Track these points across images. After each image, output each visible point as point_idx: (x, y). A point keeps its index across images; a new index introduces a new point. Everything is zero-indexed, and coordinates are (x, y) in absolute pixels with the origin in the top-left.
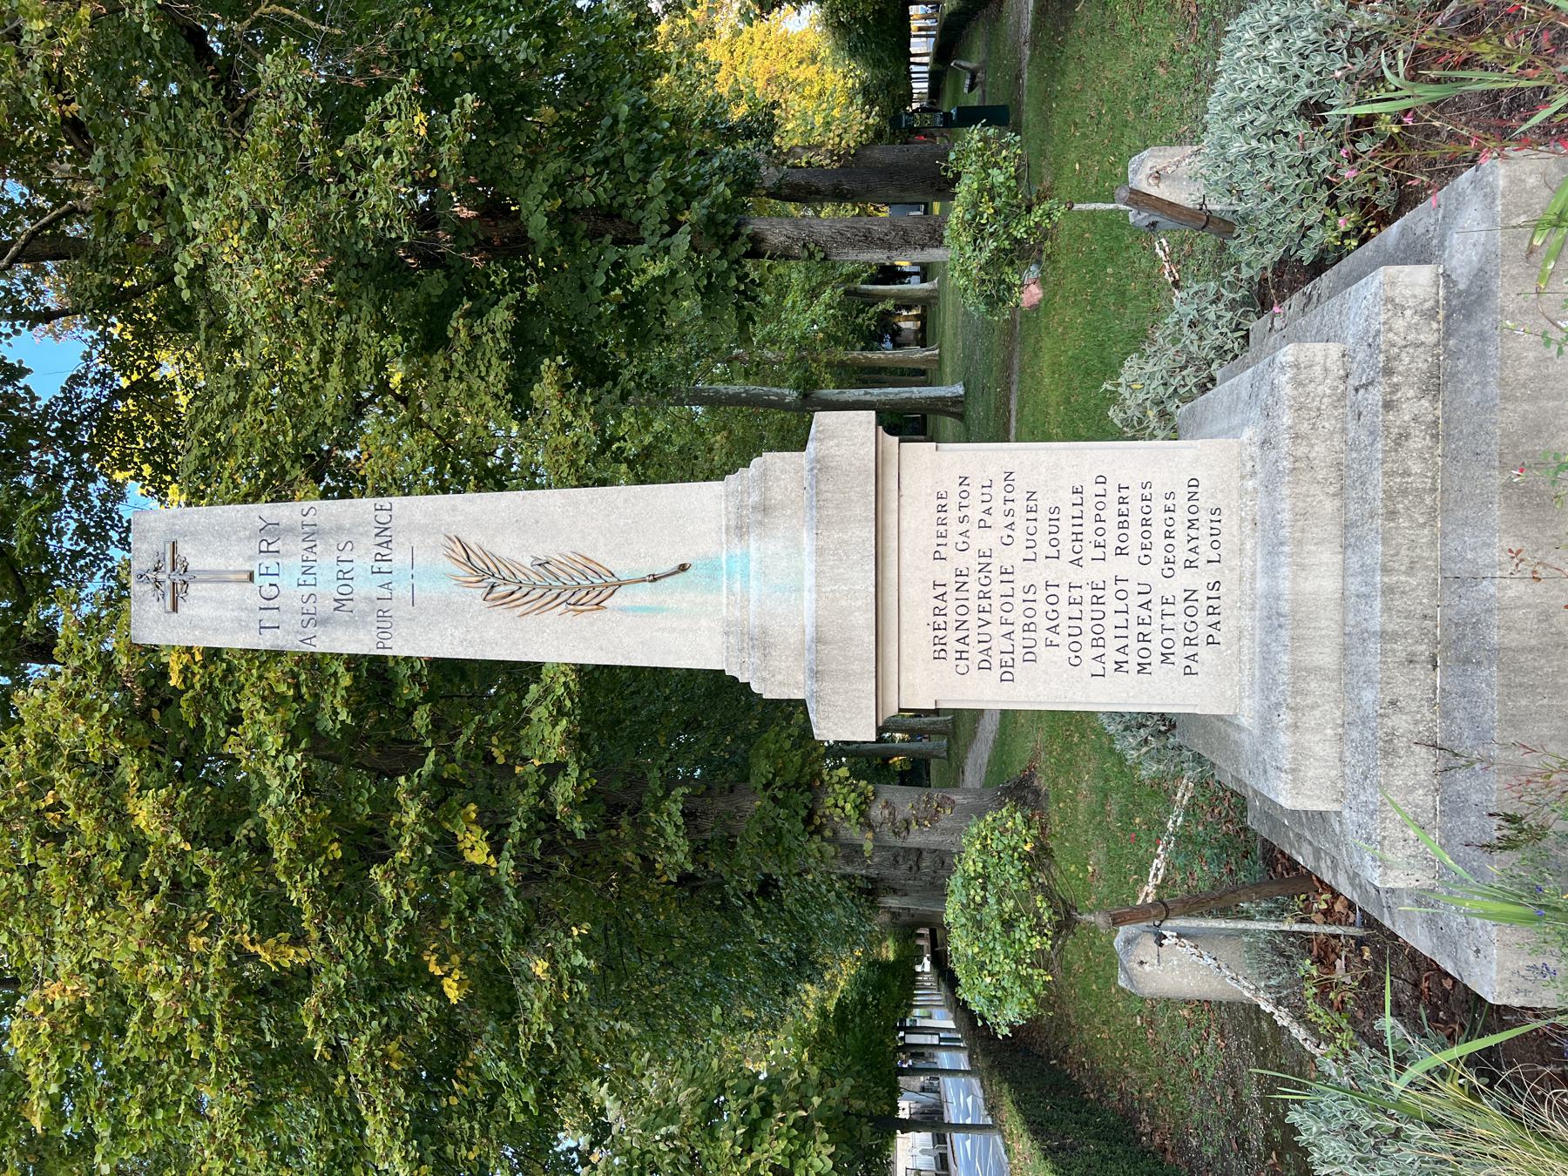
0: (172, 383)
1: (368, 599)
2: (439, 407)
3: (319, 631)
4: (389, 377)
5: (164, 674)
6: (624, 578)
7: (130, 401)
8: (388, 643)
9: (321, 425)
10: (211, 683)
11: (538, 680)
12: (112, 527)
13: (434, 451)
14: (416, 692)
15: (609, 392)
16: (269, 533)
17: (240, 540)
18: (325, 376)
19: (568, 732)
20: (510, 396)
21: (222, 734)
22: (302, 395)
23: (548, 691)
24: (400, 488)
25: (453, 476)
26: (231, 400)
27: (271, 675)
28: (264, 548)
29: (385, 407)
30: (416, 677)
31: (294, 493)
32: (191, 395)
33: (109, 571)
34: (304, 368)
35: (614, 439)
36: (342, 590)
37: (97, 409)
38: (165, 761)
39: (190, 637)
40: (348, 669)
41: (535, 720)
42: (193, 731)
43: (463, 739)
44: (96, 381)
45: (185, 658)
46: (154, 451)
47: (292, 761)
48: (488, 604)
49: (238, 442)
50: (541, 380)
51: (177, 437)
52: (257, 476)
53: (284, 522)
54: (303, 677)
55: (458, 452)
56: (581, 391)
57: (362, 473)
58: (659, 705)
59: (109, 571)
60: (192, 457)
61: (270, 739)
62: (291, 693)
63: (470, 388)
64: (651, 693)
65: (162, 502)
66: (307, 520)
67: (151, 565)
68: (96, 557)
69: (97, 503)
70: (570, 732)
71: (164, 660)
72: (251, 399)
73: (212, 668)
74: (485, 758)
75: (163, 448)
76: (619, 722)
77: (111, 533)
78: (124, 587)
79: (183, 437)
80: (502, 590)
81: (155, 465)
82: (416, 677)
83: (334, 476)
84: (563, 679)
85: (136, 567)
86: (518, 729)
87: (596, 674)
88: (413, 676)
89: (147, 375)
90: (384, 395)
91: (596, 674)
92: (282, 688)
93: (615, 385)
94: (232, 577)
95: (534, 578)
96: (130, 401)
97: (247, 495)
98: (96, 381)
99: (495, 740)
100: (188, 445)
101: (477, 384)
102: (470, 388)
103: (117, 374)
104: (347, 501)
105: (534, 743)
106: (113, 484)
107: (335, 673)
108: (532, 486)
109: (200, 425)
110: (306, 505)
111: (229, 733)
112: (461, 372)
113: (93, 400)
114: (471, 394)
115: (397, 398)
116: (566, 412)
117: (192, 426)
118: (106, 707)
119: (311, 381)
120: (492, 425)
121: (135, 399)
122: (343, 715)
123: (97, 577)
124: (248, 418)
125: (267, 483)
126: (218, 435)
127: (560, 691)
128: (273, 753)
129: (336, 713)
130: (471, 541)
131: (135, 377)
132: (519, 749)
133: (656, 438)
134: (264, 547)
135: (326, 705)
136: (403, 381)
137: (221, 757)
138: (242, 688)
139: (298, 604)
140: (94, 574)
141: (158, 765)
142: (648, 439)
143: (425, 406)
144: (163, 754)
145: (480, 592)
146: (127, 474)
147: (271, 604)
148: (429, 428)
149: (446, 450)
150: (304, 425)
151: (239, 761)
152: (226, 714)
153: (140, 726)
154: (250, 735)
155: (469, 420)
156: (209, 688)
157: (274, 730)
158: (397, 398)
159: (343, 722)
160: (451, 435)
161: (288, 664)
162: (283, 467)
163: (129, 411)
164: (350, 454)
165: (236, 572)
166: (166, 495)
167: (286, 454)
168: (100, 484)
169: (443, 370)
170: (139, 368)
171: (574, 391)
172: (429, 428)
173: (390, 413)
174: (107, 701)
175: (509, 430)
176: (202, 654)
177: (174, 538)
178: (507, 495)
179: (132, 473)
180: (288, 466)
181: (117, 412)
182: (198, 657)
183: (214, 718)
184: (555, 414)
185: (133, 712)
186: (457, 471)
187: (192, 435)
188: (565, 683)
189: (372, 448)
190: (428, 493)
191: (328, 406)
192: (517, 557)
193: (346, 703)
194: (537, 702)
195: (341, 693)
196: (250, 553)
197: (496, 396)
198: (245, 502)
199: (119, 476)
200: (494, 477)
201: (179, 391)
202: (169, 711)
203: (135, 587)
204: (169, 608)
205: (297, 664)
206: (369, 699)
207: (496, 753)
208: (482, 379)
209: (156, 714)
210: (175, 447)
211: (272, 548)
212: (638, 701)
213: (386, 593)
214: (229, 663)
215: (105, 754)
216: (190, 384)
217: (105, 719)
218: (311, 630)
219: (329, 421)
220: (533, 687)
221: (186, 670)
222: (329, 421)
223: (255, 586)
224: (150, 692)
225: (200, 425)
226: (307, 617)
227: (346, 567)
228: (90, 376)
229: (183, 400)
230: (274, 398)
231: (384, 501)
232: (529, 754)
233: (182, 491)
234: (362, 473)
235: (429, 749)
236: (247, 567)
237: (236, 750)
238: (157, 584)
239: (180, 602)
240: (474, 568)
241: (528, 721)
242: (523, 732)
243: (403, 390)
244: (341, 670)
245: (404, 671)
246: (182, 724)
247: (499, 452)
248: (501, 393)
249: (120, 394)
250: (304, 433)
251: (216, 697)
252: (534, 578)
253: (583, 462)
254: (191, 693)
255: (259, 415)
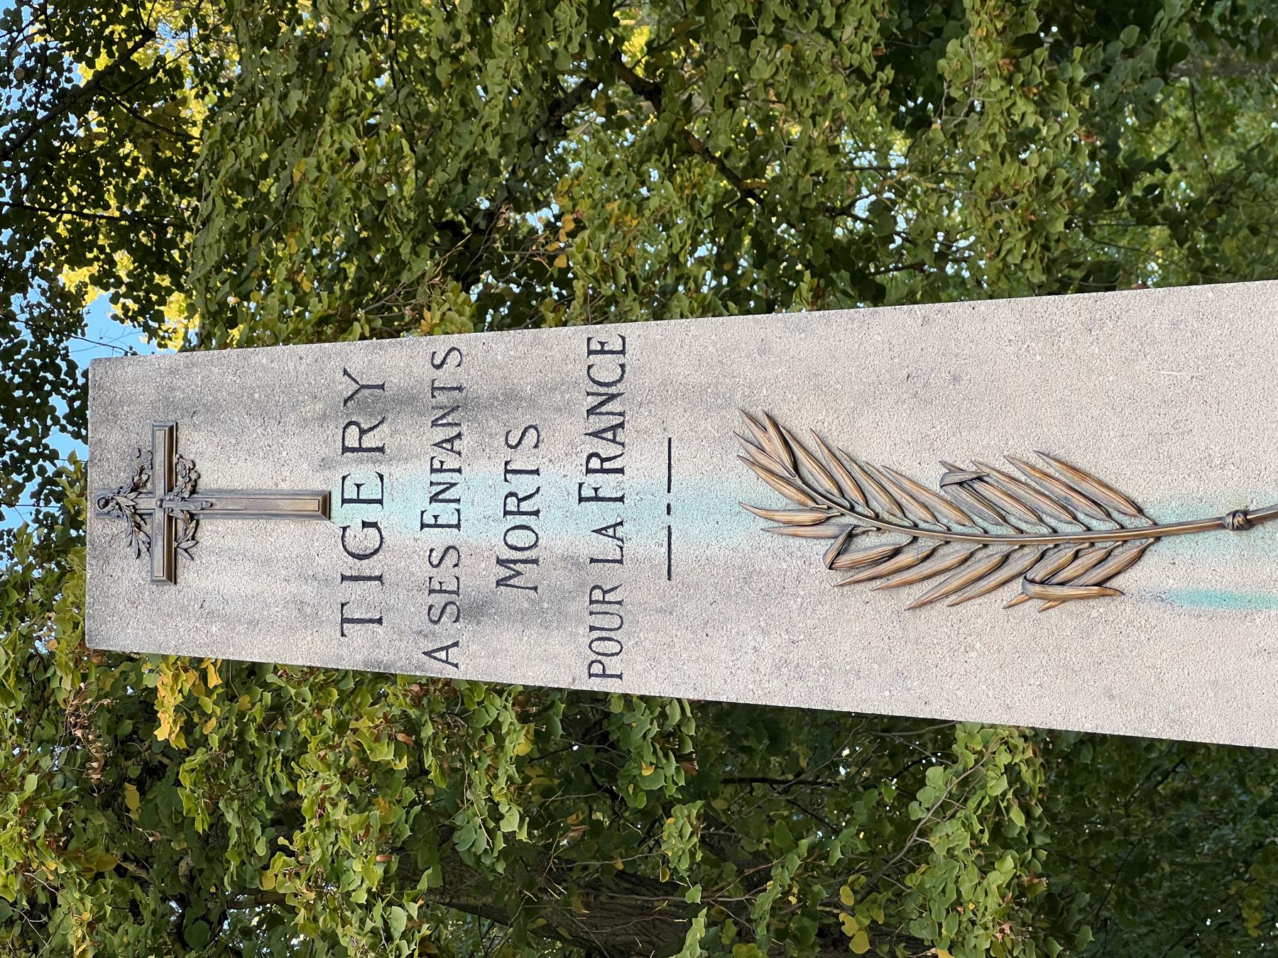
0: (176, 74)
1: (571, 562)
2: (730, 104)
3: (464, 632)
4: (620, 40)
5: (146, 709)
6: (1168, 517)
7: (93, 115)
8: (613, 665)
9: (475, 158)
10: (241, 734)
11: (949, 758)
12: (55, 389)
13: (716, 207)
14: (670, 777)
15: (1129, 53)
16: (364, 407)
17: (305, 422)
18: (484, 46)
19: (1018, 890)
20: (888, 74)
21: (261, 849)
22: (436, 88)
23: (967, 784)
24: (645, 297)
25: (758, 264)
26: (293, 107)
27: (364, 724)
28: (352, 441)
29: (611, 109)
30: (668, 739)
31: (419, 310)
32: (212, 98)
33: (48, 481)
34: (441, 29)
35: (1139, 165)
36: (514, 538)
37: (30, 133)
38: (150, 901)
39: (201, 638)
40: (523, 718)
41: (940, 852)
42: (204, 839)
43: (773, 890)
44: (27, 74)
45: (189, 680)
46: (137, 222)
47: (399, 920)
48: (838, 577)
49: (306, 200)
50: (964, 29)
51: (182, 189)
52: (340, 275)
53: (395, 381)
54: (428, 731)
55: (768, 208)
56: (1059, 52)
57: (561, 262)
58: (1245, 826)
59: (48, 481)
60: (213, 235)
61: (357, 866)
62: (403, 765)
63: (798, 57)
64: (1225, 795)
65: (152, 333)
66: (444, 377)
67: (124, 478)
68: (23, 450)
69: (27, 335)
70: (1022, 890)
71: (149, 681)
72: (333, 104)
73: (244, 700)
74: (822, 933)
75: (154, 218)
76: (1143, 865)
77: (55, 400)
78: (75, 520)
79: (195, 190)
80: (871, 544)
81: (140, 254)
82: (668, 739)
83: (501, 273)
84: (1004, 759)
85: (98, 481)
86: (902, 870)
87: (1086, 757)
88: (664, 737)
89: (126, 56)
90: (609, 83)
91: (1086, 757)
92: (385, 753)
93: (1146, 31)
94: (286, 505)
95: (949, 516)
96: (93, 115)
97: (323, 321)
98: (27, 74)
99: (846, 897)
100: (204, 208)
101: (814, 47)
102: (798, 57)
103: (67, 57)
104: (530, 334)
105: (939, 910)
106: (58, 295)
107: (497, 724)
108: (935, 291)
109: (229, 165)
110: (441, 343)
111: (274, 848)
112: (779, 22)
113: (22, 114)
114: (800, 72)
115: (640, 87)
116: (1022, 106)
117: (214, 162)
118: (32, 781)
119: (455, 58)
120: (846, 141)
121: (103, 109)
122: (512, 822)
123: (25, 497)
124: (326, 148)
125: (362, 286)
126: (264, 186)
127: (998, 785)
128: (362, 898)
129: (497, 816)
130: (801, 424)
131: (102, 62)
132: (903, 918)
133: (1244, 158)
134: (352, 439)
135: (476, 796)
136: (651, 48)
137: (260, 897)
138: (303, 746)
139: (421, 570)
140: (19, 488)
141: (135, 908)
142: (1223, 161)
143: (698, 102)
144: (144, 884)
145: (821, 549)
146: (83, 274)
147: (366, 567)
148: (707, 154)
149: (742, 203)
150: (440, 160)
151: (293, 911)
152: (271, 805)
153: (101, 821)
154: (316, 854)
155: (795, 131)
156: (237, 745)
157: (369, 846)
158: (640, 87)
159: (509, 837)
160: (755, 168)
161: (398, 703)
162: (394, 253)
163: (91, 137)
164: (536, 219)
165: (295, 495)
166: (159, 317)
167: (401, 225)
168: (34, 295)
169: (740, 19)
170: (110, 42)
171: (1042, 53)
172: (707, 154)
173: (621, 124)
174: (35, 768)
175: (883, 150)
176: (220, 672)
177: (171, 418)
178: (886, 313)
179: (95, 268)
180: (405, 251)
181: (69, 138)
182: (214, 680)
183: (246, 812)
184: (994, 112)
185: (87, 791)
186: (765, 254)
187: (213, 187)
188: (1009, 768)
189: (584, 207)
190: (706, 309)
191: (492, 115)
192: (909, 467)
193: (519, 793)
194: (944, 811)
195: (507, 769)
196: (325, 452)
197: (857, 73)
198: (319, 337)
199: (69, 278)
200: (849, 265)
201: (189, 88)
202: (159, 790)
203: (97, 527)
204: (160, 573)
205: (417, 702)
206: (567, 783)
207: (850, 925)
208: (827, 34)
209: (131, 795)
210: (178, 212)
211: (370, 441)
212: (1191, 816)
213: (607, 547)
214: (278, 692)
215: (27, 884)
216: (209, 75)
217: (29, 807)
218: (448, 630)
219: (493, 147)
220: (935, 775)
221: (190, 710)
222: (493, 147)
223: (334, 526)
224: (123, 746)
225: (229, 165)
226: (440, 600)
227: (523, 485)
228: (16, 63)
229: (196, 110)
230: (379, 98)
231: (608, 333)
232: (924, 934)
233: (191, 310)
234: (561, 262)
235: (693, 910)
236: (318, 484)
237: (287, 888)
238: (138, 518)
239: (183, 559)
240: (808, 490)
241: (922, 852)
242: (911, 881)
243: (650, 68)
244: (509, 718)
245: (646, 726)
246: (182, 823)
247: (861, 209)
248: (869, 68)
249: (74, 101)
250: (440, 177)
251: (250, 766)
252: (949, 516)
253: (1060, 227)
254: (199, 757)
255: (350, 140)
